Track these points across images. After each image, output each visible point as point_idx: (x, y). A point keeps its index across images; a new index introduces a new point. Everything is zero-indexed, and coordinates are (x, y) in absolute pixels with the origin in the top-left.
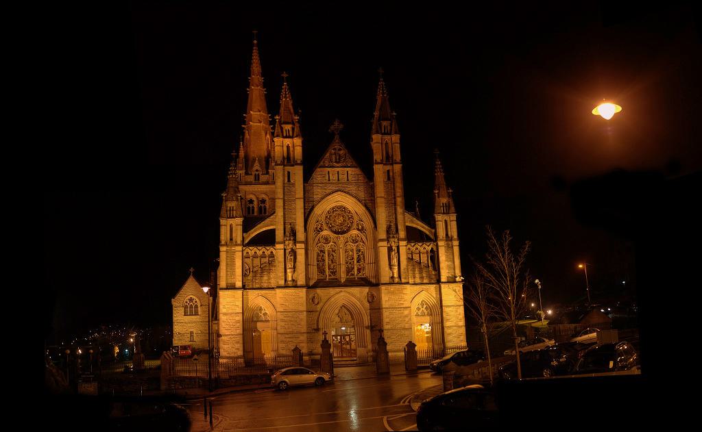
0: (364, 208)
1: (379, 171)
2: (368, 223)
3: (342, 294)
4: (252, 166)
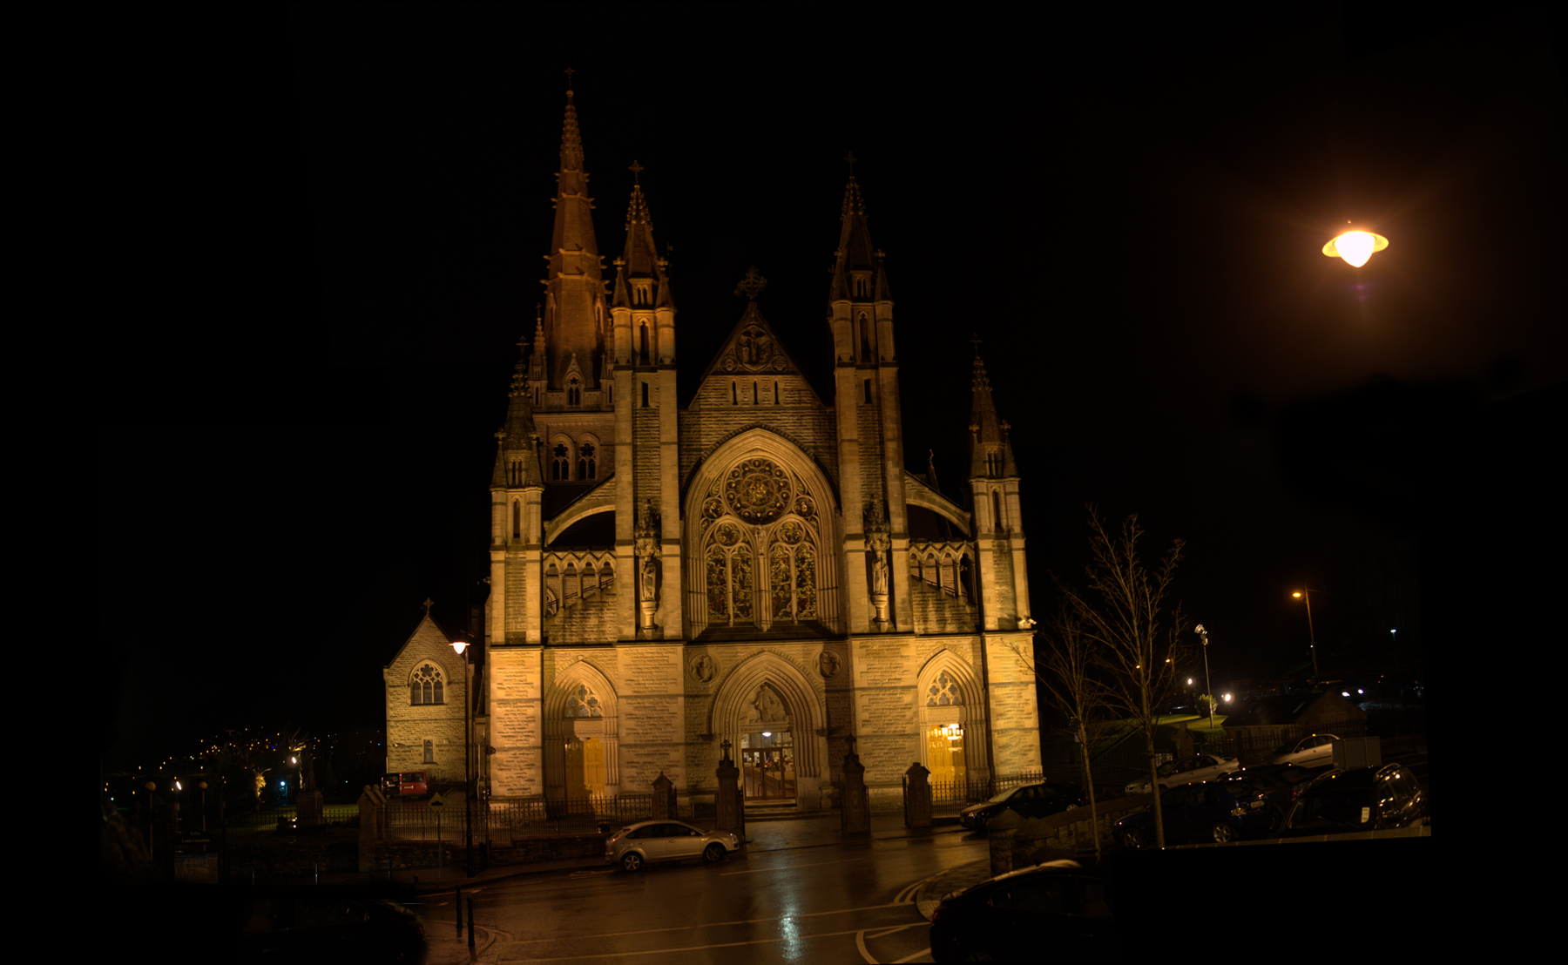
3: (763, 657)
4: (564, 371)
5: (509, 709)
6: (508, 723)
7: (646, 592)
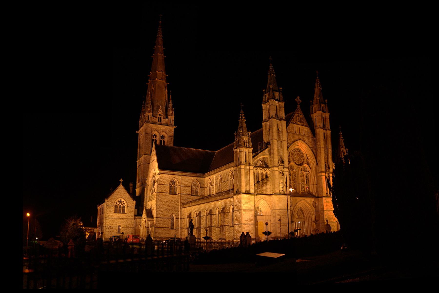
0: (312, 152)
1: (320, 132)
2: (312, 161)
3: (302, 201)
4: (157, 111)
5: (246, 212)
6: (246, 216)
7: (281, 181)
